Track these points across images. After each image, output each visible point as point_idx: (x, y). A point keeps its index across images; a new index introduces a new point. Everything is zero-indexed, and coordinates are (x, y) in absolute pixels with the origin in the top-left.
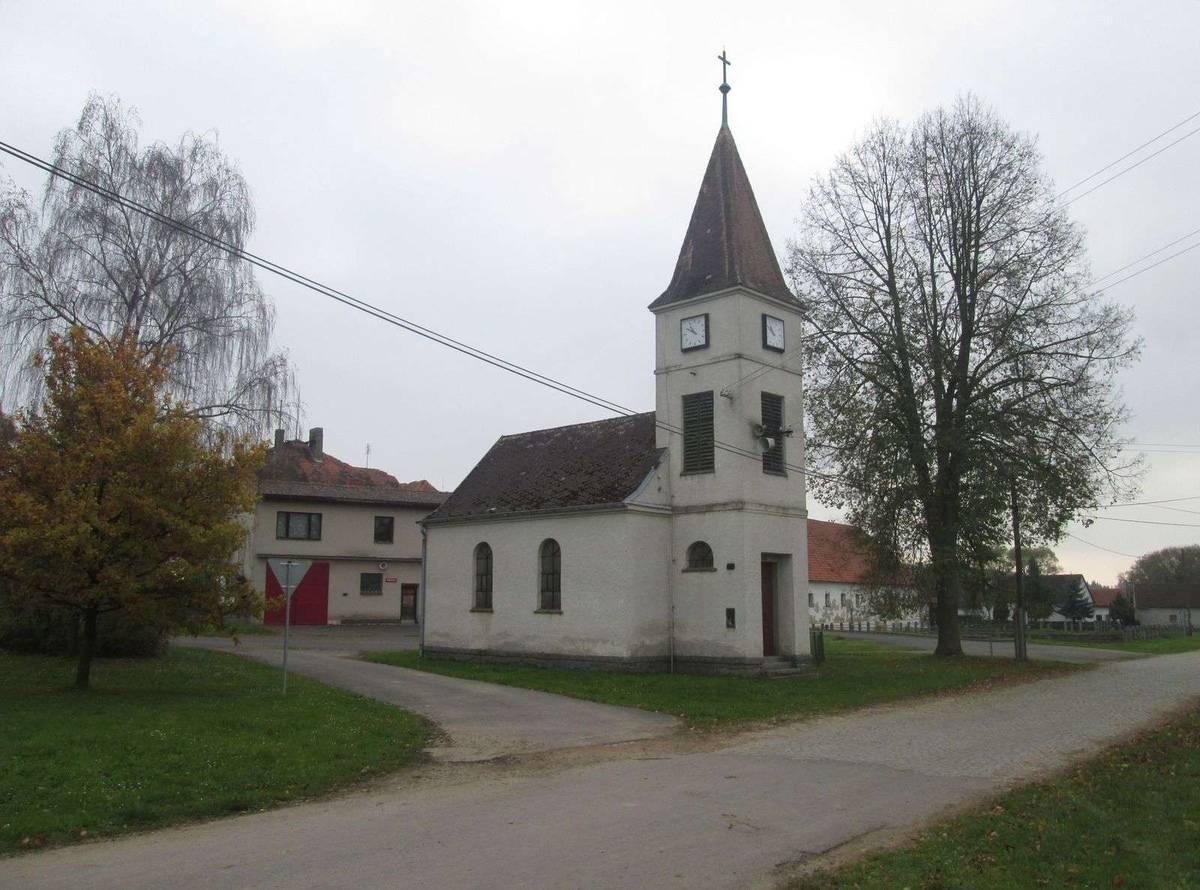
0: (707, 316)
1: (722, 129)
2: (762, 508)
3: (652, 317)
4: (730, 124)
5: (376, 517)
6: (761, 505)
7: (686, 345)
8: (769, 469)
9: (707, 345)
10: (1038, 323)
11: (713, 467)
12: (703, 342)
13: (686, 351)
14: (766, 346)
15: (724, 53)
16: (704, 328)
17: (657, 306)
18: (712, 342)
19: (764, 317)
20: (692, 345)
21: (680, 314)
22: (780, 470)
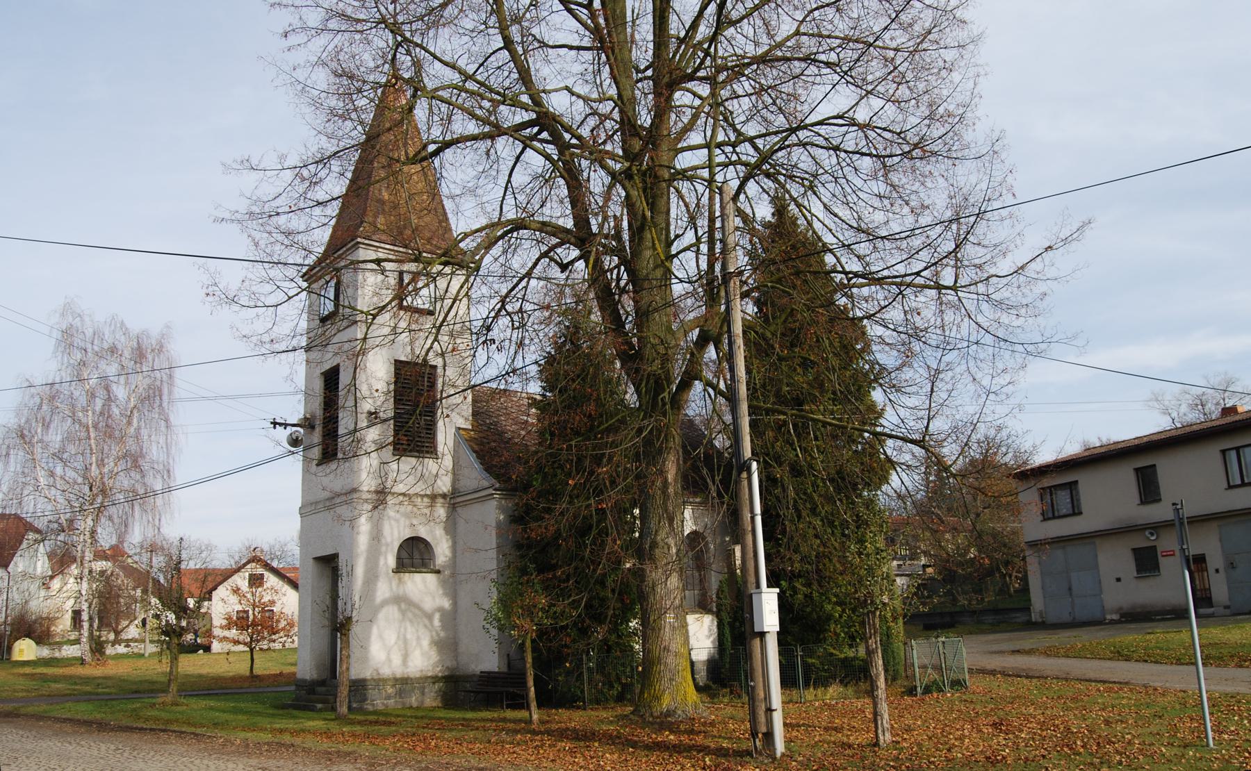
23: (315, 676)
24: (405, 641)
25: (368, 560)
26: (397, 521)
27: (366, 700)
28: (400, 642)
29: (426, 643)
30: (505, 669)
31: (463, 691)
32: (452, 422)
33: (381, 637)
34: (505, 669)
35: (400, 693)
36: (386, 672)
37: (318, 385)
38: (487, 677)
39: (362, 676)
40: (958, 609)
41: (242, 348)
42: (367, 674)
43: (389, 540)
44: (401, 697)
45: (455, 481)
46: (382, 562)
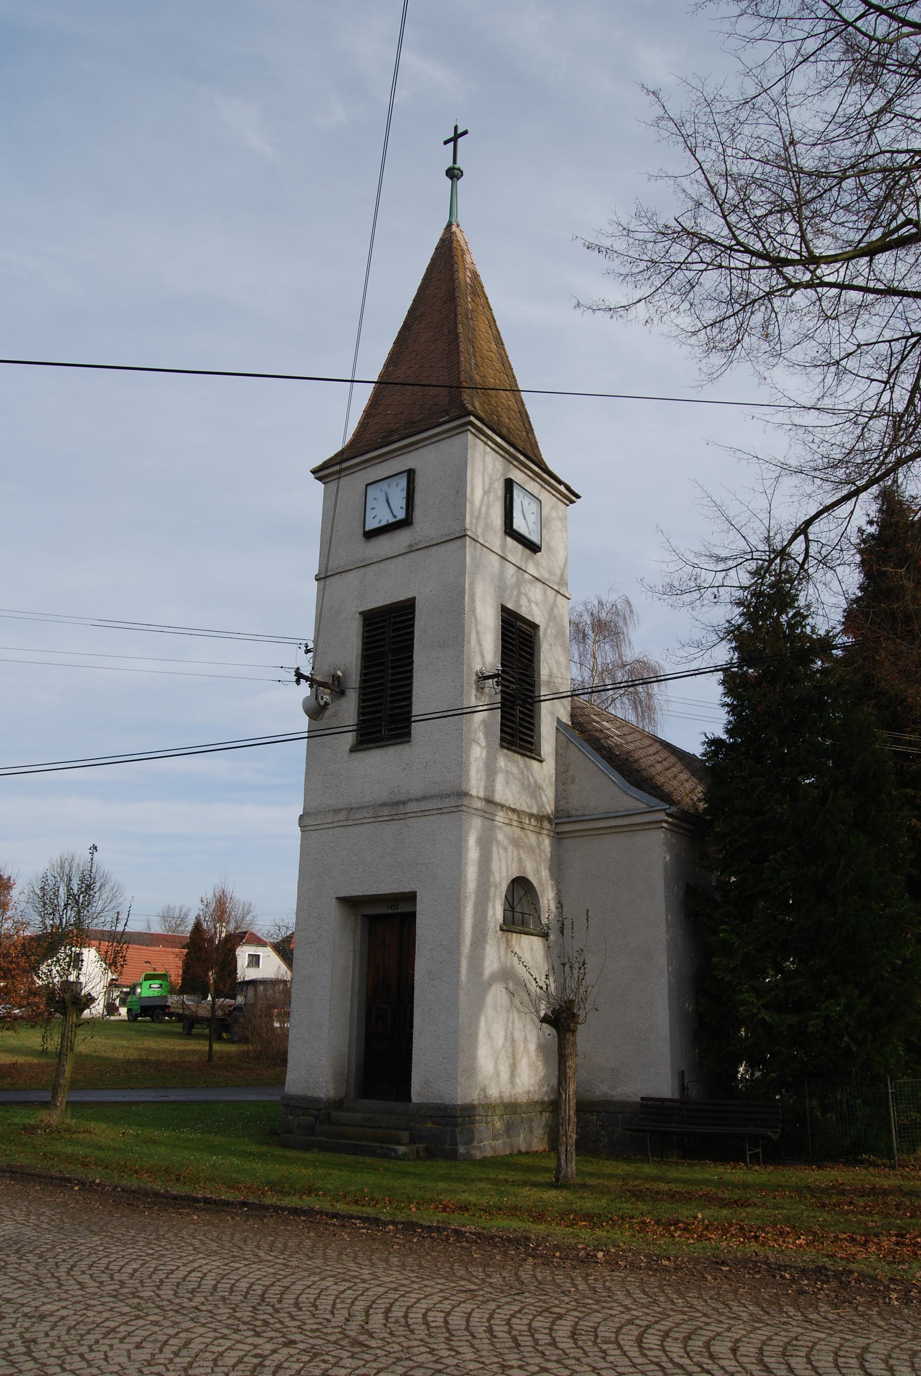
0: (411, 474)
1: (442, 241)
2: (342, 816)
3: (320, 486)
4: (462, 217)
5: (363, 916)
6: (337, 811)
7: (371, 525)
8: (511, 743)
9: (406, 523)
10: (671, 586)
11: (409, 734)
12: (401, 515)
13: (370, 535)
14: (509, 530)
15: (465, 133)
16: (404, 494)
17: (323, 472)
18: (418, 514)
19: (509, 485)
20: (384, 523)
21: (360, 479)
22: (531, 751)
23: (332, 1094)
24: (513, 1041)
25: (476, 907)
26: (505, 849)
27: (472, 1140)
28: (508, 1044)
29: (532, 1046)
30: (677, 1096)
31: (598, 1130)
32: (551, 716)
33: (489, 1035)
34: (677, 1096)
35: (510, 1128)
36: (494, 1092)
37: (348, 655)
38: (651, 1107)
39: (468, 1100)
40: (81, 1022)
41: (811, 582)
42: (474, 1097)
43: (498, 879)
44: (509, 1136)
45: (559, 796)
46: (490, 913)
